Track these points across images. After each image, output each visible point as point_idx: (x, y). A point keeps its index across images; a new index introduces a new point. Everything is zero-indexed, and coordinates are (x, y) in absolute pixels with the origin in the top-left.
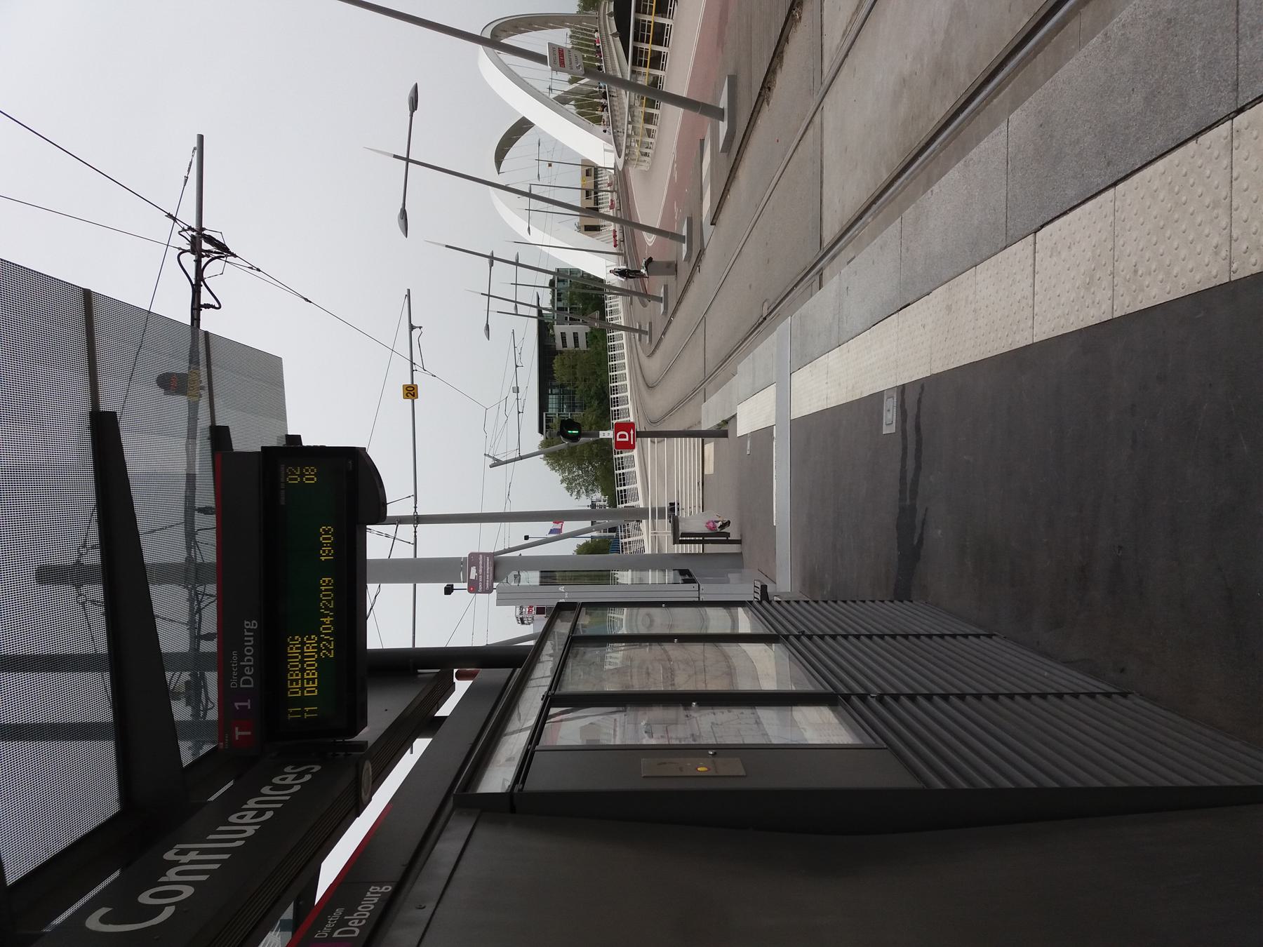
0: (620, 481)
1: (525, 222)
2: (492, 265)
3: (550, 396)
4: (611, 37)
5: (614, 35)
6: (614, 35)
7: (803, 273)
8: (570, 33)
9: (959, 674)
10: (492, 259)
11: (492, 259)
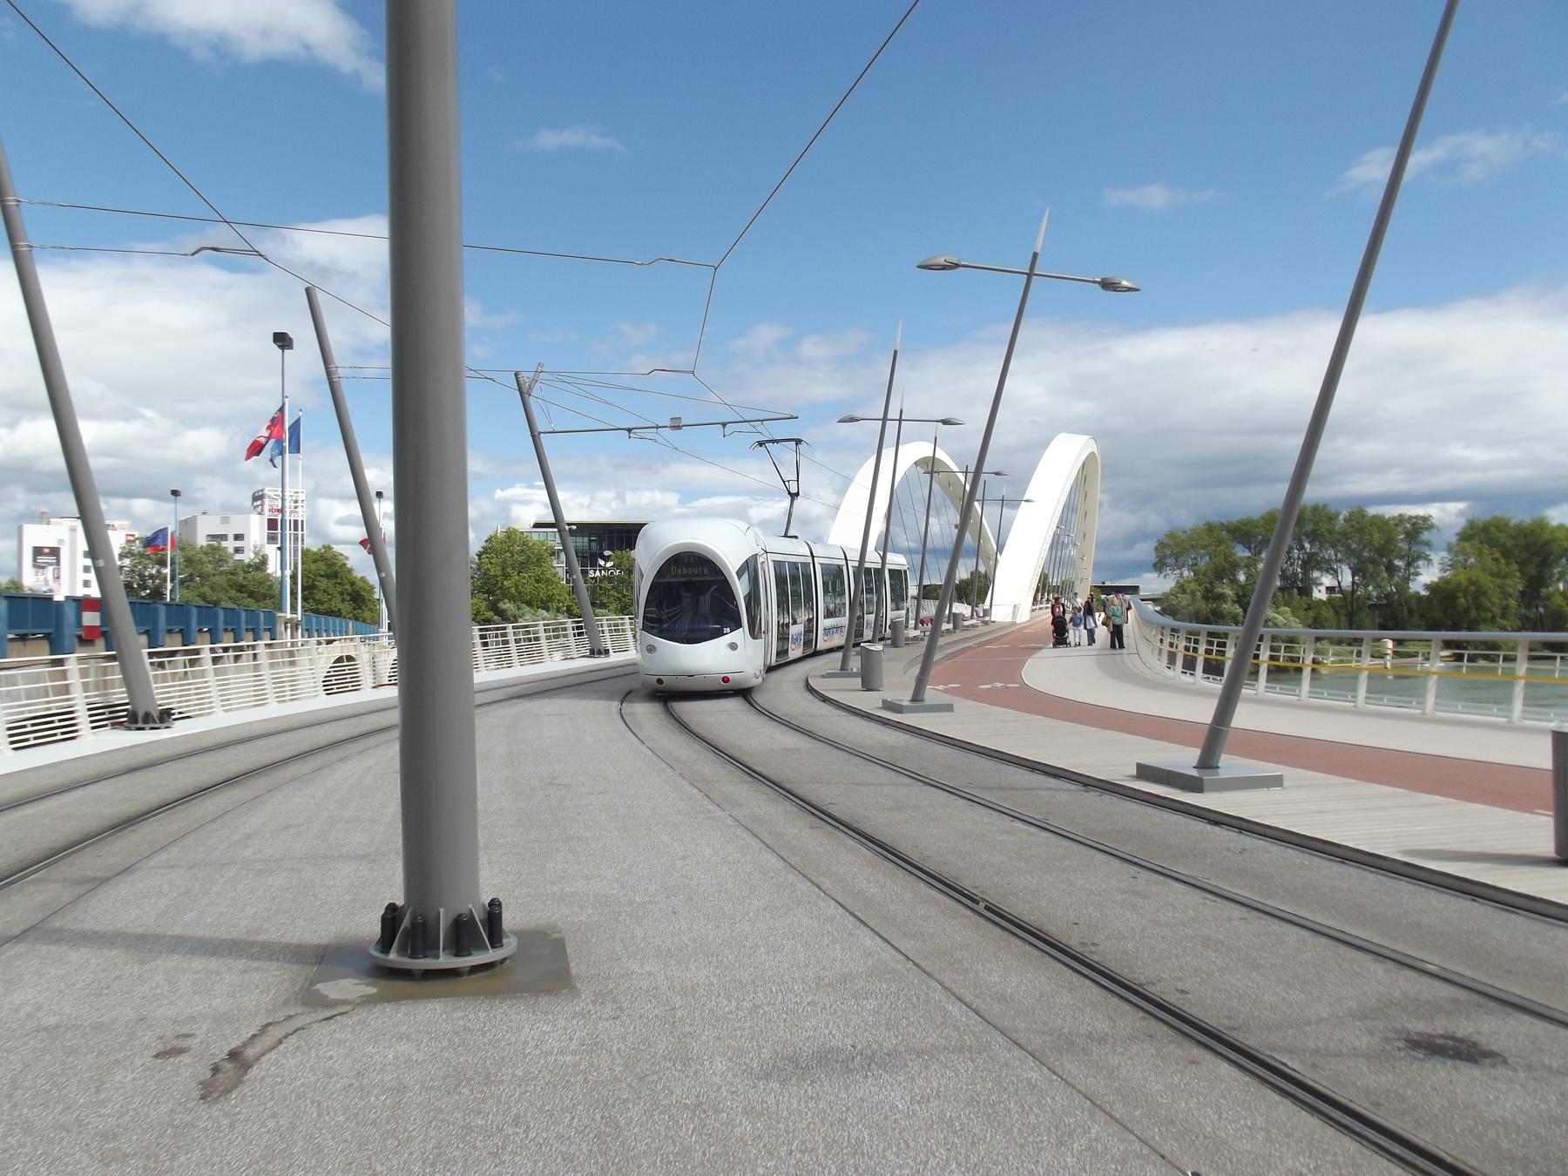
3: (586, 539)
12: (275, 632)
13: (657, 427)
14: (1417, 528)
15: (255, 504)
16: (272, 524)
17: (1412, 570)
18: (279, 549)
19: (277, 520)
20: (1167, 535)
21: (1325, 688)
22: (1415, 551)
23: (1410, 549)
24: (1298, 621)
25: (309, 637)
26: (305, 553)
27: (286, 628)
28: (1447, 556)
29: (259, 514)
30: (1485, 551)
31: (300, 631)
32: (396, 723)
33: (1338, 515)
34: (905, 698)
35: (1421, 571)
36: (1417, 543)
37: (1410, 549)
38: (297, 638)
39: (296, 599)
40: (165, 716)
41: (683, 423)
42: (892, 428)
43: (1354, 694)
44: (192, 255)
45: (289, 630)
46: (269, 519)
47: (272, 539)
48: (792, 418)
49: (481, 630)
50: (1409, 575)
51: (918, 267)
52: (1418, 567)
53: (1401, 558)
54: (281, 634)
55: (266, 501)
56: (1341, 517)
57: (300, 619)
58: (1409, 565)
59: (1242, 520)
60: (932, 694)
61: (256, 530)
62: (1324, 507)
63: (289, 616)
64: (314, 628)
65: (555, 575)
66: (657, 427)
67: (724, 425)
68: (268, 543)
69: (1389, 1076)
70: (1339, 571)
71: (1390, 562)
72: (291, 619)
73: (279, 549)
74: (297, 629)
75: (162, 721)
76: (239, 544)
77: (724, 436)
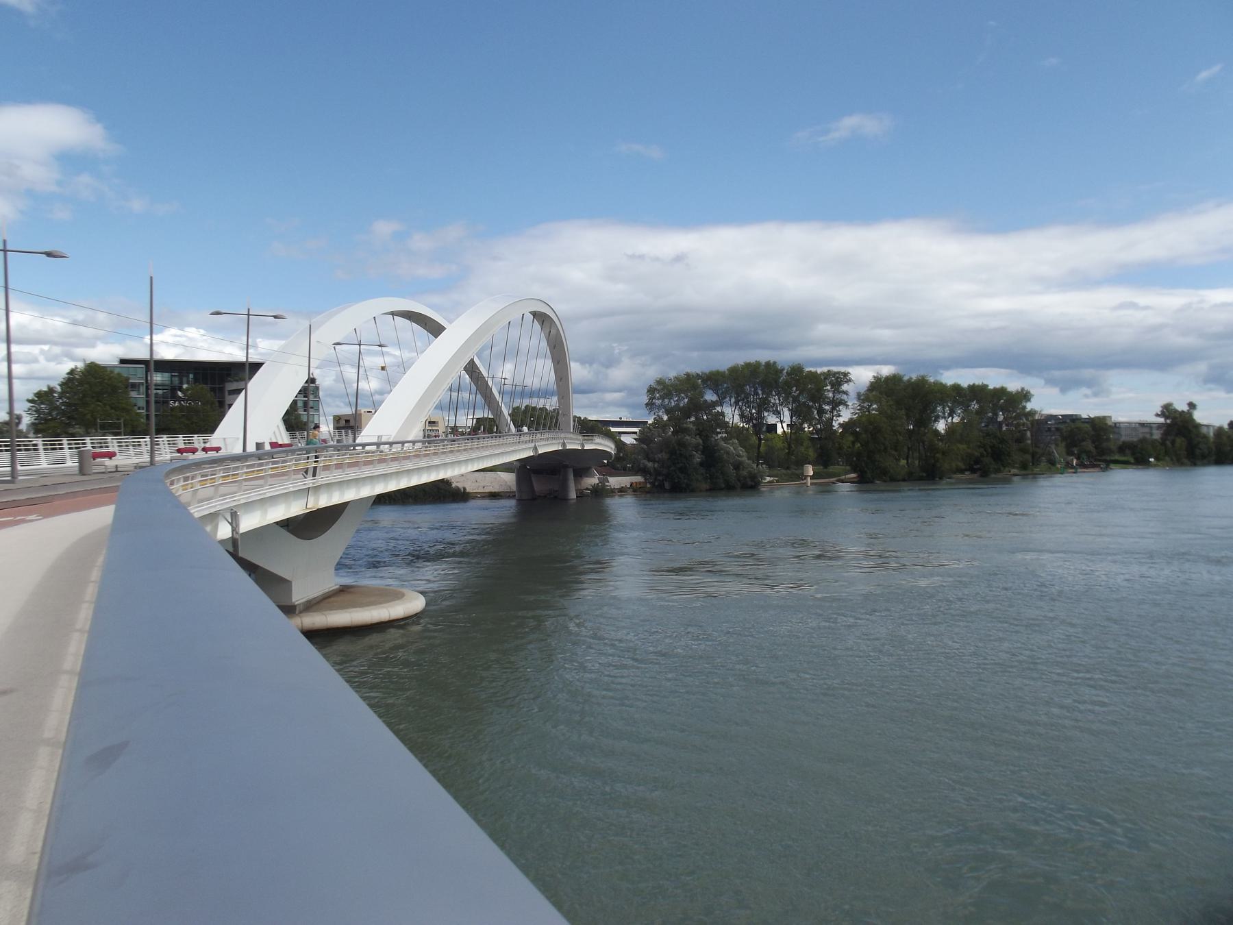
14: (839, 380)
17: (835, 413)
20: (657, 381)
22: (837, 399)
23: (834, 396)
24: (744, 450)
28: (856, 402)
30: (883, 399)
33: (783, 370)
35: (841, 413)
36: (839, 393)
37: (834, 396)
49: (68, 440)
50: (833, 417)
52: (840, 411)
53: (828, 404)
56: (785, 371)
58: (833, 409)
59: (712, 371)
62: (775, 363)
69: (937, 844)
70: (781, 413)
71: (820, 406)
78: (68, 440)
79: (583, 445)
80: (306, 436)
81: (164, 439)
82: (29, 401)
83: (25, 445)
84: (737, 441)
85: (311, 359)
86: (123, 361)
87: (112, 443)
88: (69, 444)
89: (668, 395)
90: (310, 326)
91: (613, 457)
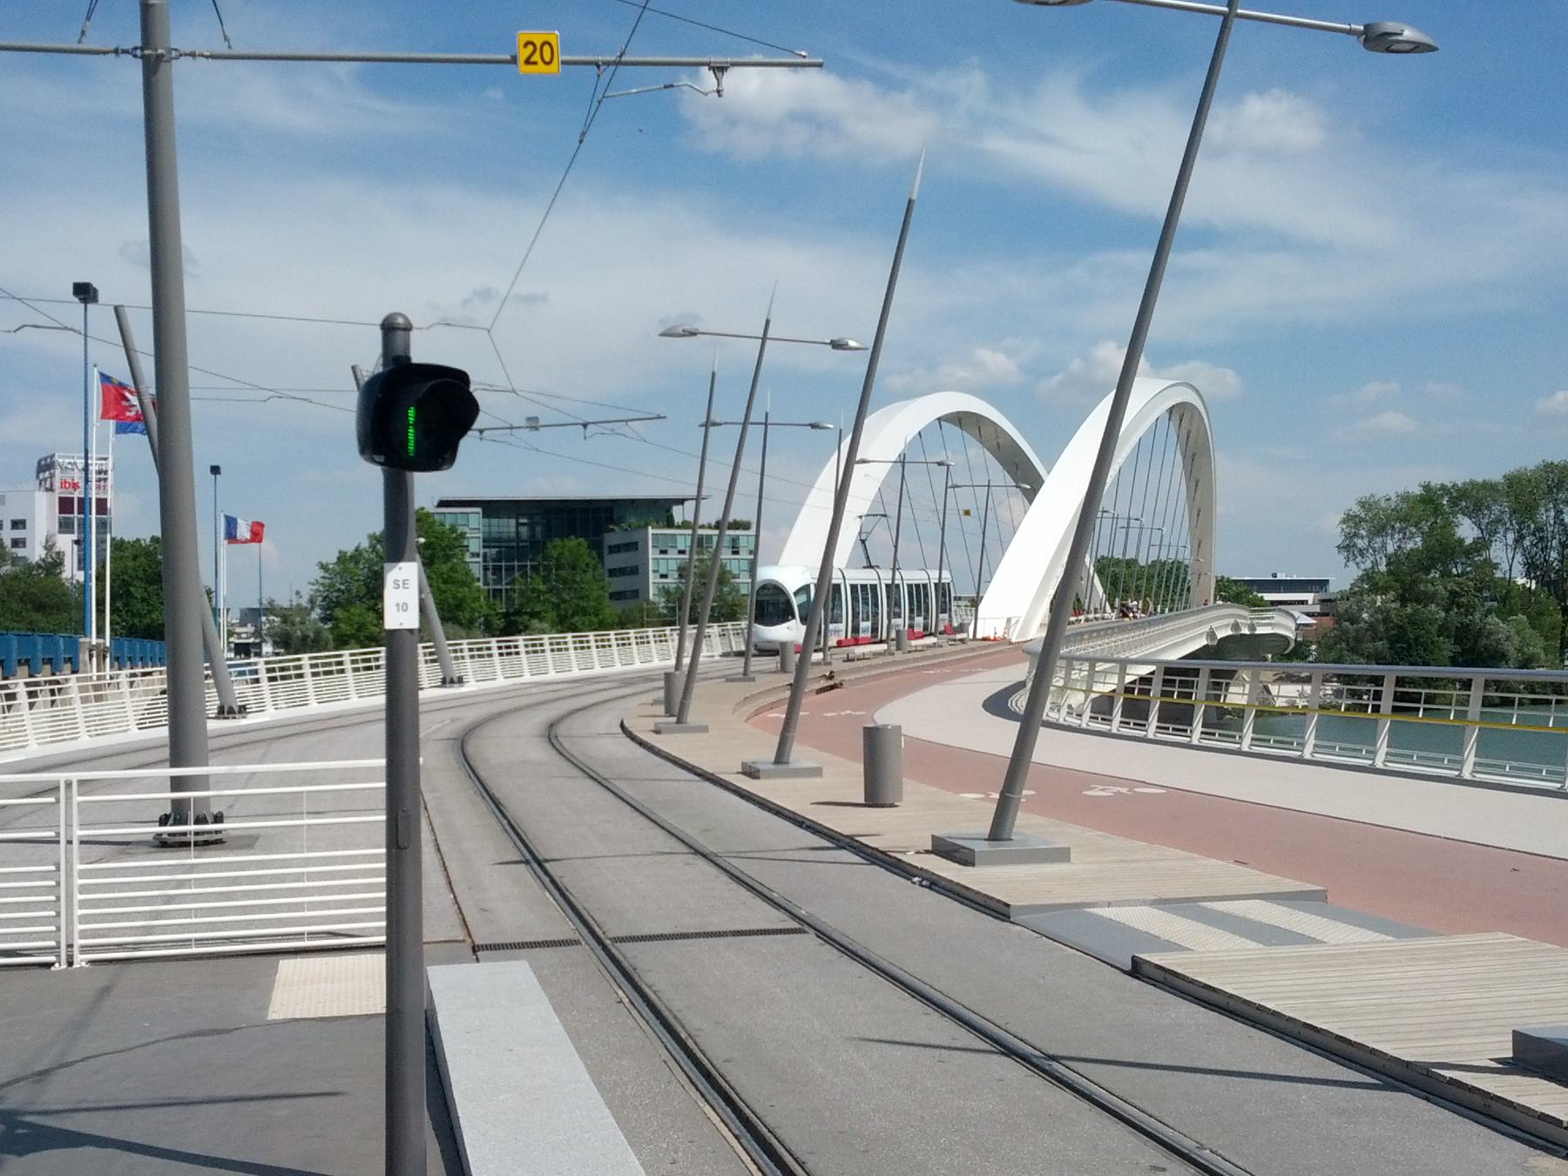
0: (479, 649)
1: (868, 504)
2: (715, 424)
3: (513, 522)
4: (1206, 628)
5: (1211, 634)
6: (1211, 634)
7: (475, 779)
8: (362, 547)
9: (1417, 1044)
10: (708, 424)
11: (585, 426)
12: (77, 663)
13: (511, 428)
15: (41, 476)
16: (65, 505)
18: (77, 542)
19: (73, 499)
21: (1363, 744)
25: (120, 669)
26: (118, 546)
27: (91, 656)
29: (47, 490)
31: (108, 660)
32: (164, 743)
34: (764, 753)
38: (105, 671)
39: (104, 611)
40: (243, 710)
41: (541, 423)
42: (754, 433)
43: (1301, 741)
44: (15, 331)
45: (94, 659)
46: (60, 498)
47: (65, 526)
48: (659, 417)
51: (663, 334)
54: (85, 664)
55: (57, 471)
57: (108, 644)
60: (800, 755)
61: (42, 514)
63: (94, 641)
64: (126, 654)
65: (468, 573)
66: (511, 428)
67: (585, 426)
68: (60, 532)
72: (98, 645)
73: (77, 542)
74: (105, 657)
75: (240, 712)
76: (18, 534)
77: (585, 438)
78: (311, 658)
79: (1252, 627)
80: (382, 662)
81: (714, 630)
82: (323, 567)
83: (282, 669)
84: (1524, 618)
85: (765, 478)
86: (443, 504)
87: (672, 635)
88: (353, 662)
89: (1380, 530)
90: (768, 322)
91: (1292, 645)
